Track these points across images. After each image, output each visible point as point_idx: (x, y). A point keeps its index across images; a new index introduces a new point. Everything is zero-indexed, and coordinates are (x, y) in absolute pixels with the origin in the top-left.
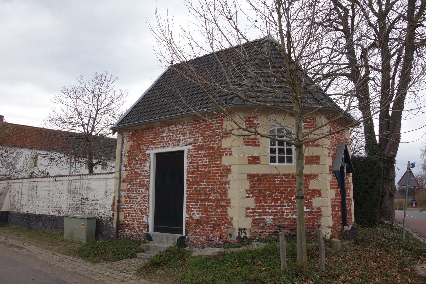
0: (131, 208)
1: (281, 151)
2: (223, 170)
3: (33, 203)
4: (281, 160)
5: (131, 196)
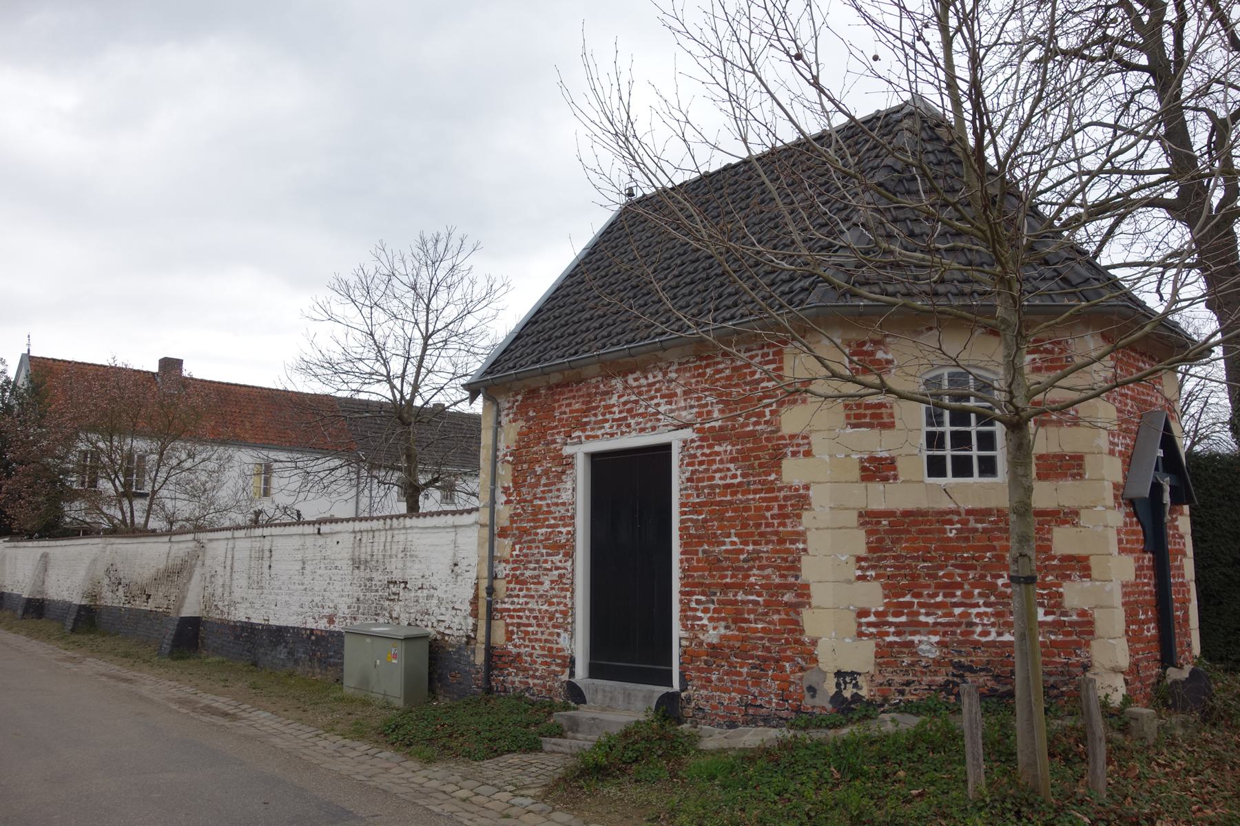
1: (961, 440)
2: (786, 498)
4: (962, 467)
5: (522, 574)
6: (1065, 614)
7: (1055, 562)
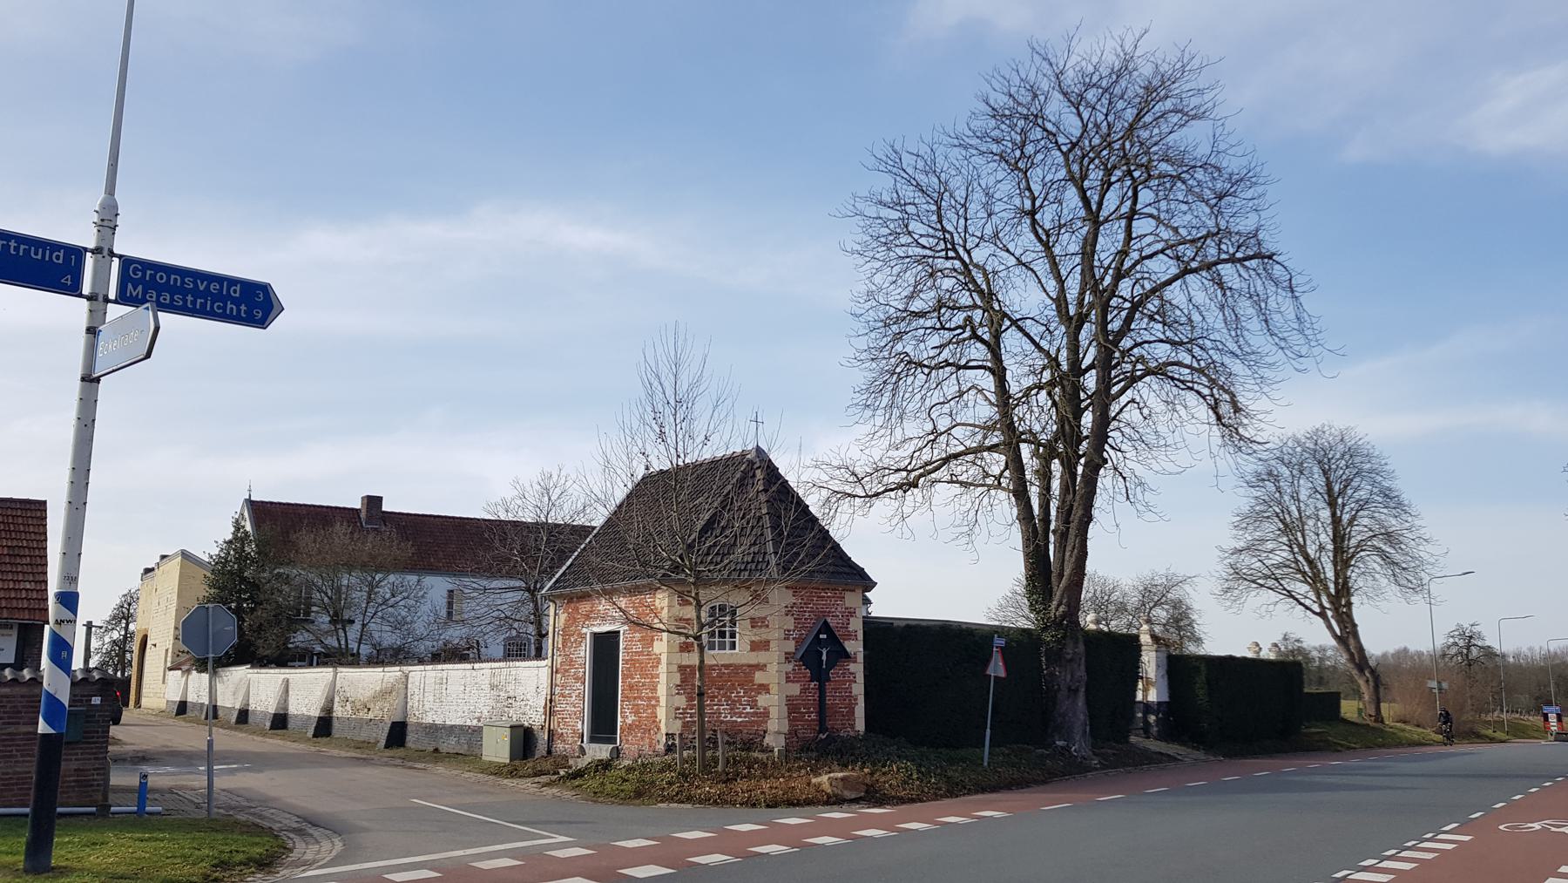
1: (722, 635)
4: (722, 646)
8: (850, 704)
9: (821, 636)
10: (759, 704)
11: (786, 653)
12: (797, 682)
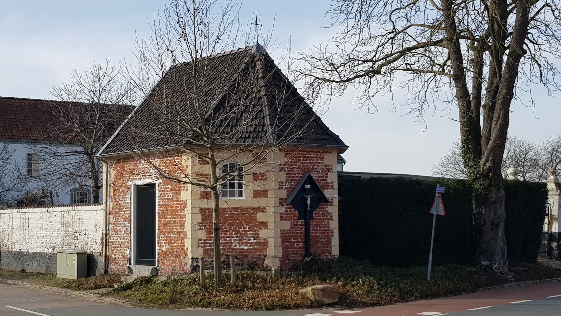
0: (116, 242)
2: (182, 204)
3: (26, 239)
5: (116, 228)
6: (259, 240)
7: (258, 224)
8: (328, 236)
9: (306, 186)
10: (260, 236)
11: (280, 199)
12: (289, 220)
